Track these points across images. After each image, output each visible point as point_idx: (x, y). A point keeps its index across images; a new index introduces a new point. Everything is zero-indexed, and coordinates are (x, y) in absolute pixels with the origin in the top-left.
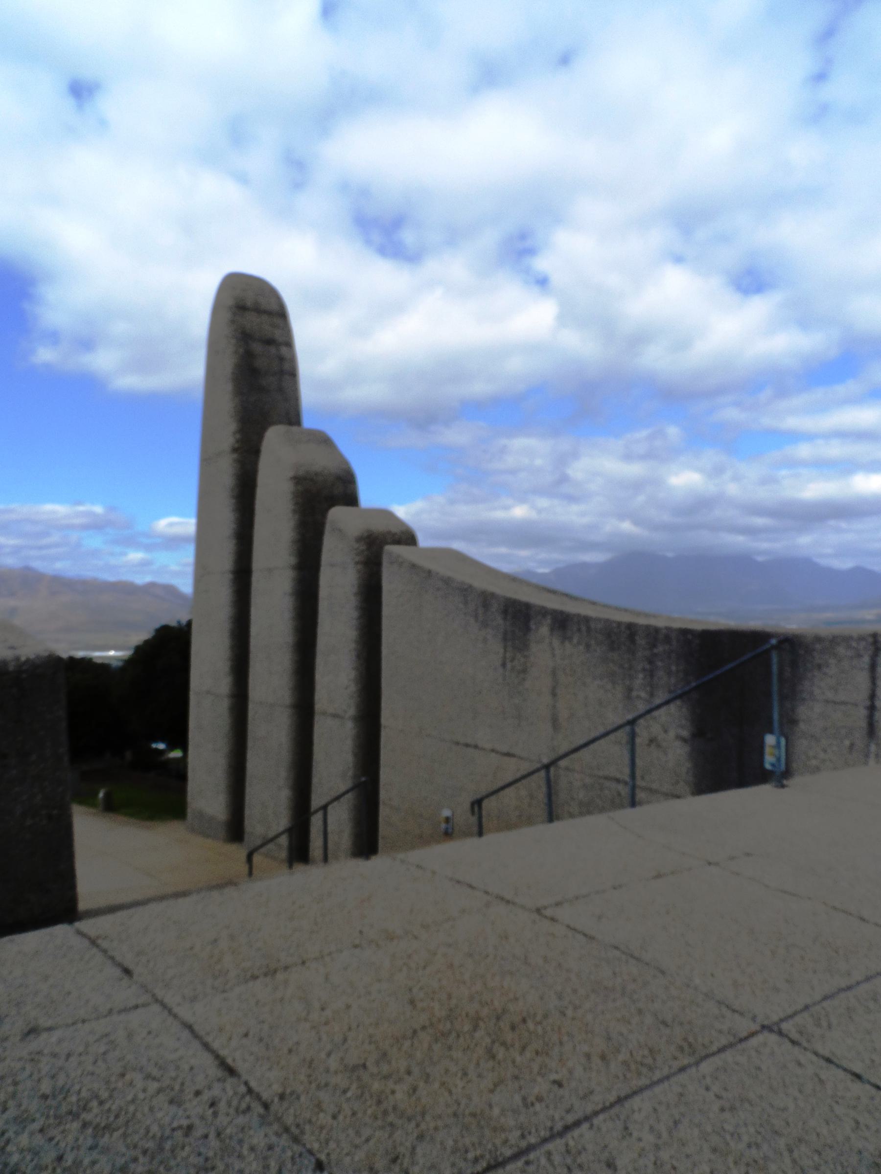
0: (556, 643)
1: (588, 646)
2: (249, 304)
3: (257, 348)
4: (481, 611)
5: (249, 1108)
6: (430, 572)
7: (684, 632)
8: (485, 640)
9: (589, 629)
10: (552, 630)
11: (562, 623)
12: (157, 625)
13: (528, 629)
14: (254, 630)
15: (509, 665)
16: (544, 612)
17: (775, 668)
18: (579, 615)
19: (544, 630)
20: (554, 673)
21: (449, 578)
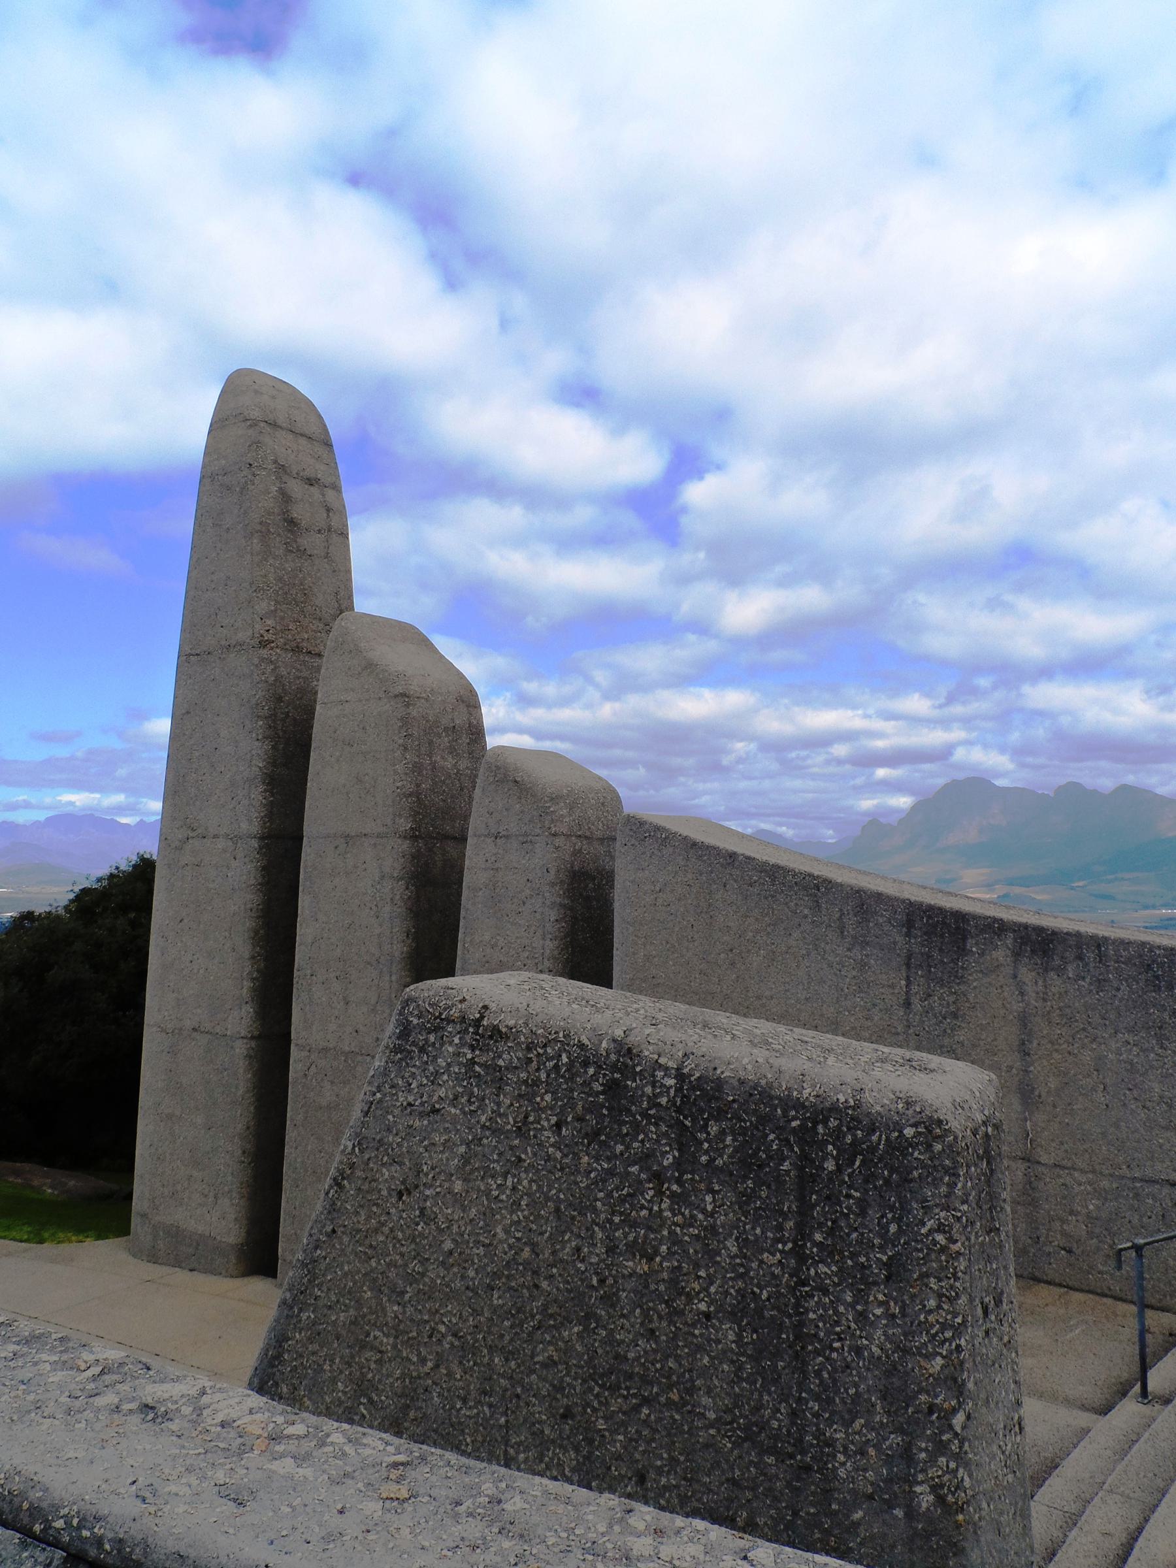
0: (1027, 975)
1: (1100, 983)
2: (281, 421)
3: (296, 488)
4: (851, 921)
5: (1118, 1127)
6: (732, 855)
7: (911, 904)
8: (863, 966)
9: (1101, 958)
10: (1017, 955)
11: (1040, 945)
12: (26, 909)
13: (963, 951)
14: (305, 931)
15: (917, 1005)
16: (996, 928)
17: (709, 786)
18: (1078, 935)
19: (1001, 954)
20: (1024, 1020)
21: (777, 867)
